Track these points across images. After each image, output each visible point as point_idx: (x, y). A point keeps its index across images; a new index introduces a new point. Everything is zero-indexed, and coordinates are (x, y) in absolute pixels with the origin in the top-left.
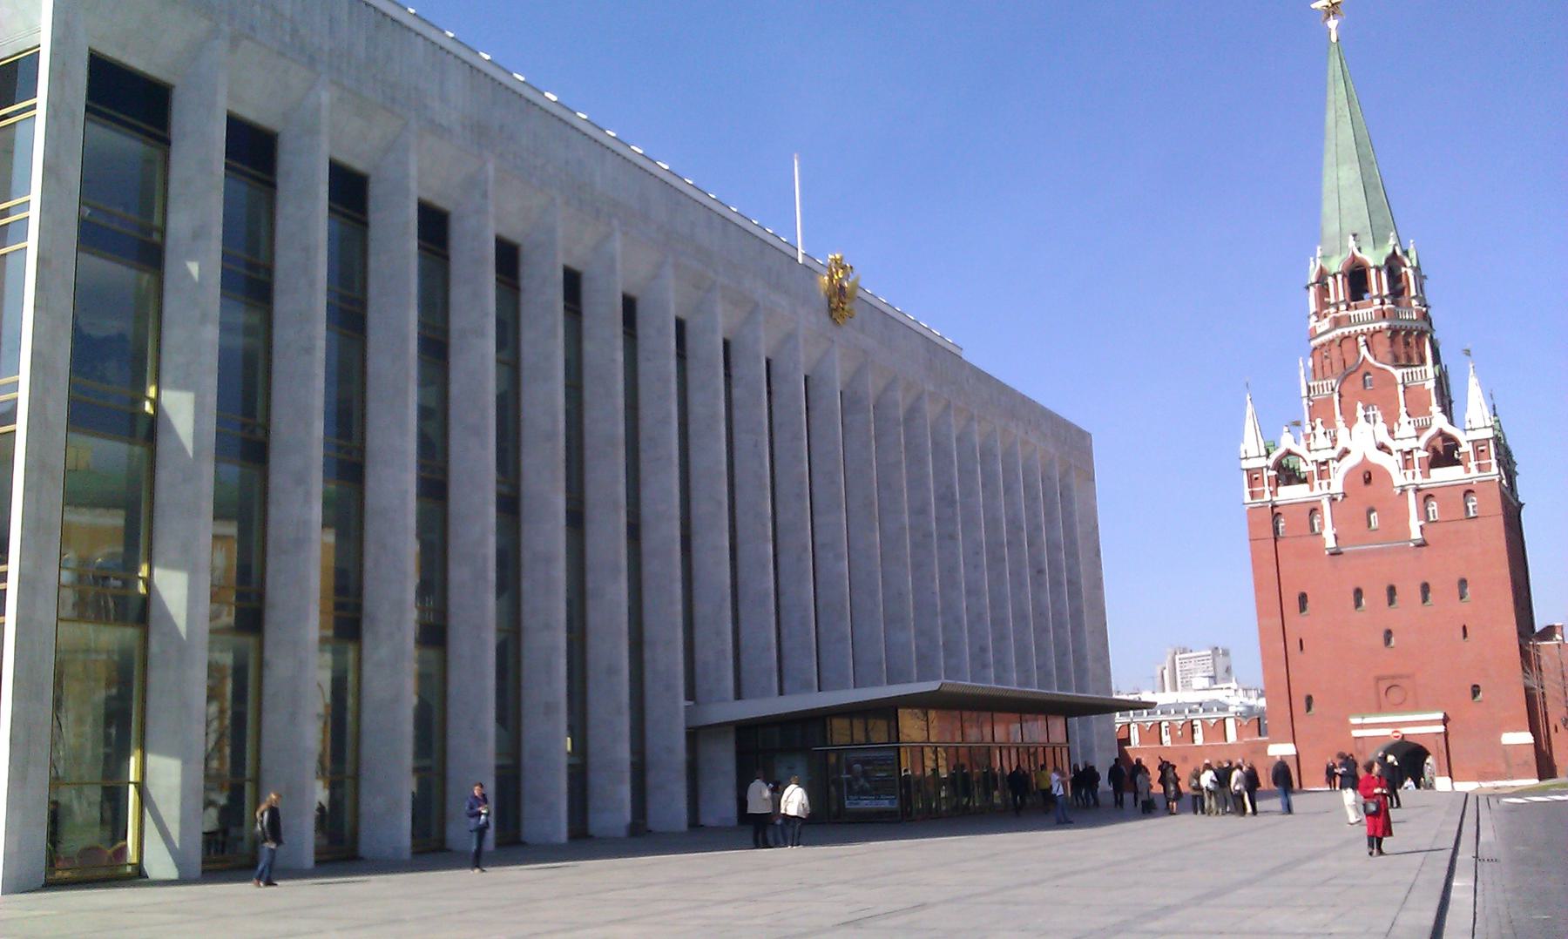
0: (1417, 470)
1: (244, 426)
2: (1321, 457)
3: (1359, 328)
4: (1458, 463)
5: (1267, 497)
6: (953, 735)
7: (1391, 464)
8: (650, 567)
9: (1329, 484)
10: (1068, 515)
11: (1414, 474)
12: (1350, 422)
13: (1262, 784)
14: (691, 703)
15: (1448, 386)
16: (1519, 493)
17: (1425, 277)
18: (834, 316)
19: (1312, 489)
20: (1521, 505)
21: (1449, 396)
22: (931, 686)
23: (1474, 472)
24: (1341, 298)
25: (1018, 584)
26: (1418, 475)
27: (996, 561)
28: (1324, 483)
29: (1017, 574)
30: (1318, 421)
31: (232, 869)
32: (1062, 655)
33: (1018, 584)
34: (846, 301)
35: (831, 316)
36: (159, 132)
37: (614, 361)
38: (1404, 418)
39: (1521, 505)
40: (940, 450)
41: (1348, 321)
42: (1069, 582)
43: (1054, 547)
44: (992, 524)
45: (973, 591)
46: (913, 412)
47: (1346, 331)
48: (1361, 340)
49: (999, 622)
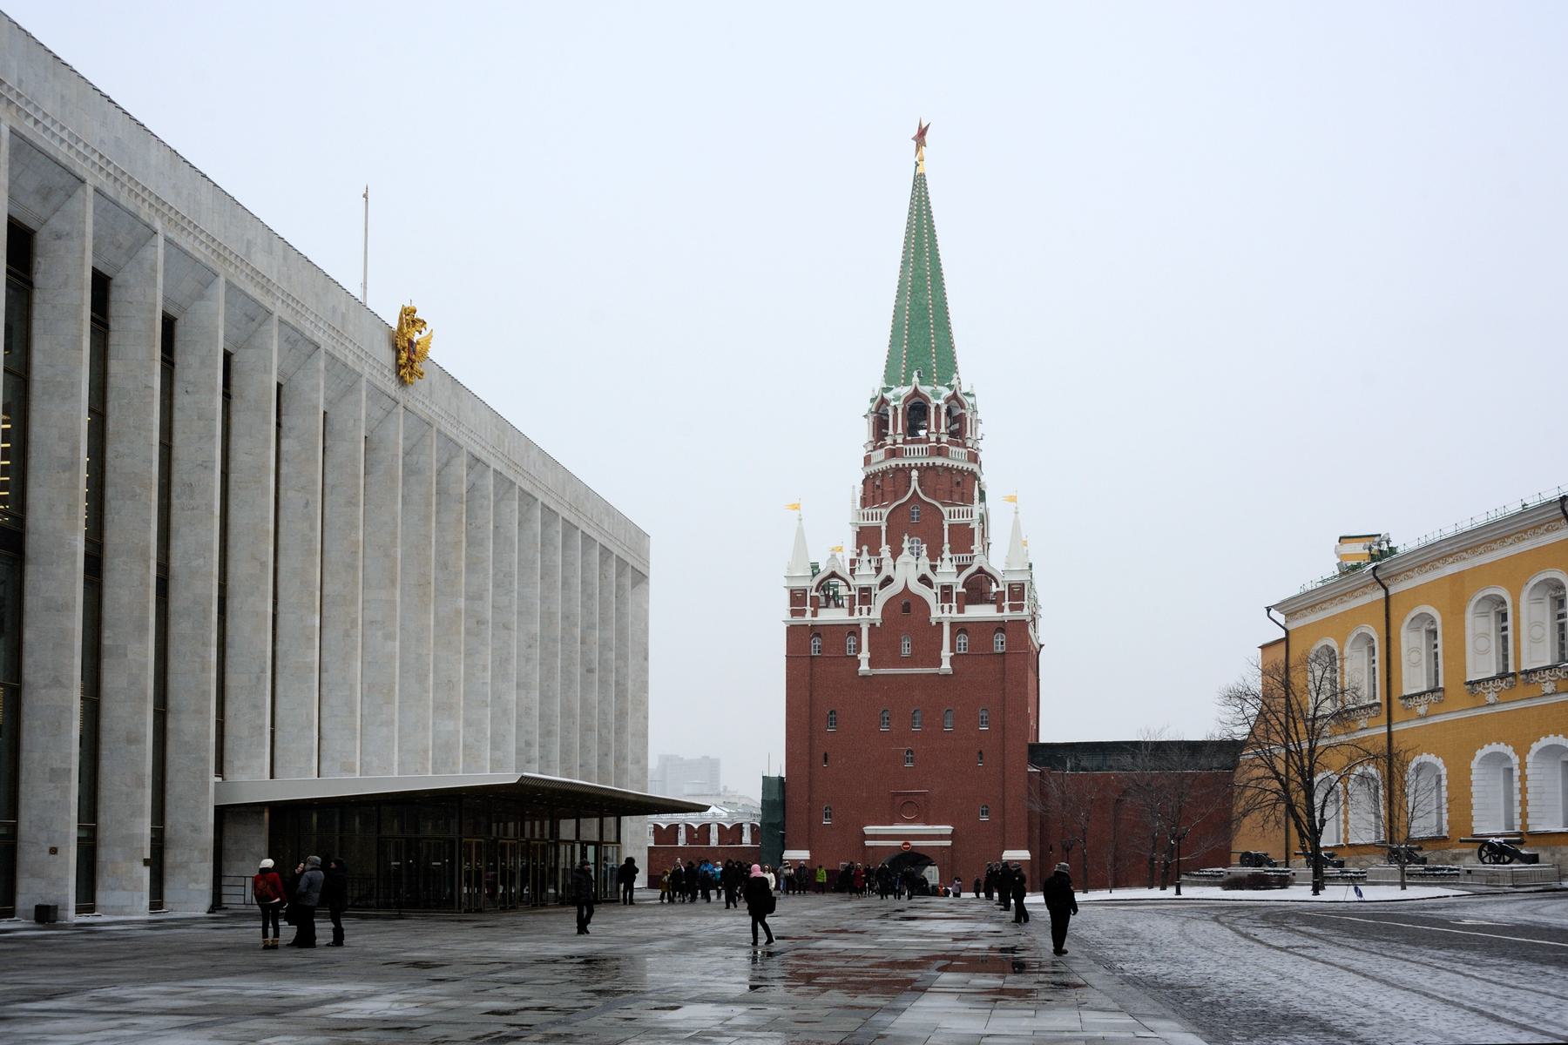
0: (954, 604)
2: (864, 583)
5: (808, 615)
7: (929, 595)
8: (179, 627)
9: (869, 610)
11: (951, 607)
12: (896, 553)
14: (220, 779)
18: (401, 373)
19: (851, 613)
26: (955, 610)
28: (865, 608)
29: (567, 672)
30: (865, 548)
35: (398, 373)
37: (149, 387)
42: (617, 683)
43: (604, 645)
47: (900, 462)
48: (915, 474)
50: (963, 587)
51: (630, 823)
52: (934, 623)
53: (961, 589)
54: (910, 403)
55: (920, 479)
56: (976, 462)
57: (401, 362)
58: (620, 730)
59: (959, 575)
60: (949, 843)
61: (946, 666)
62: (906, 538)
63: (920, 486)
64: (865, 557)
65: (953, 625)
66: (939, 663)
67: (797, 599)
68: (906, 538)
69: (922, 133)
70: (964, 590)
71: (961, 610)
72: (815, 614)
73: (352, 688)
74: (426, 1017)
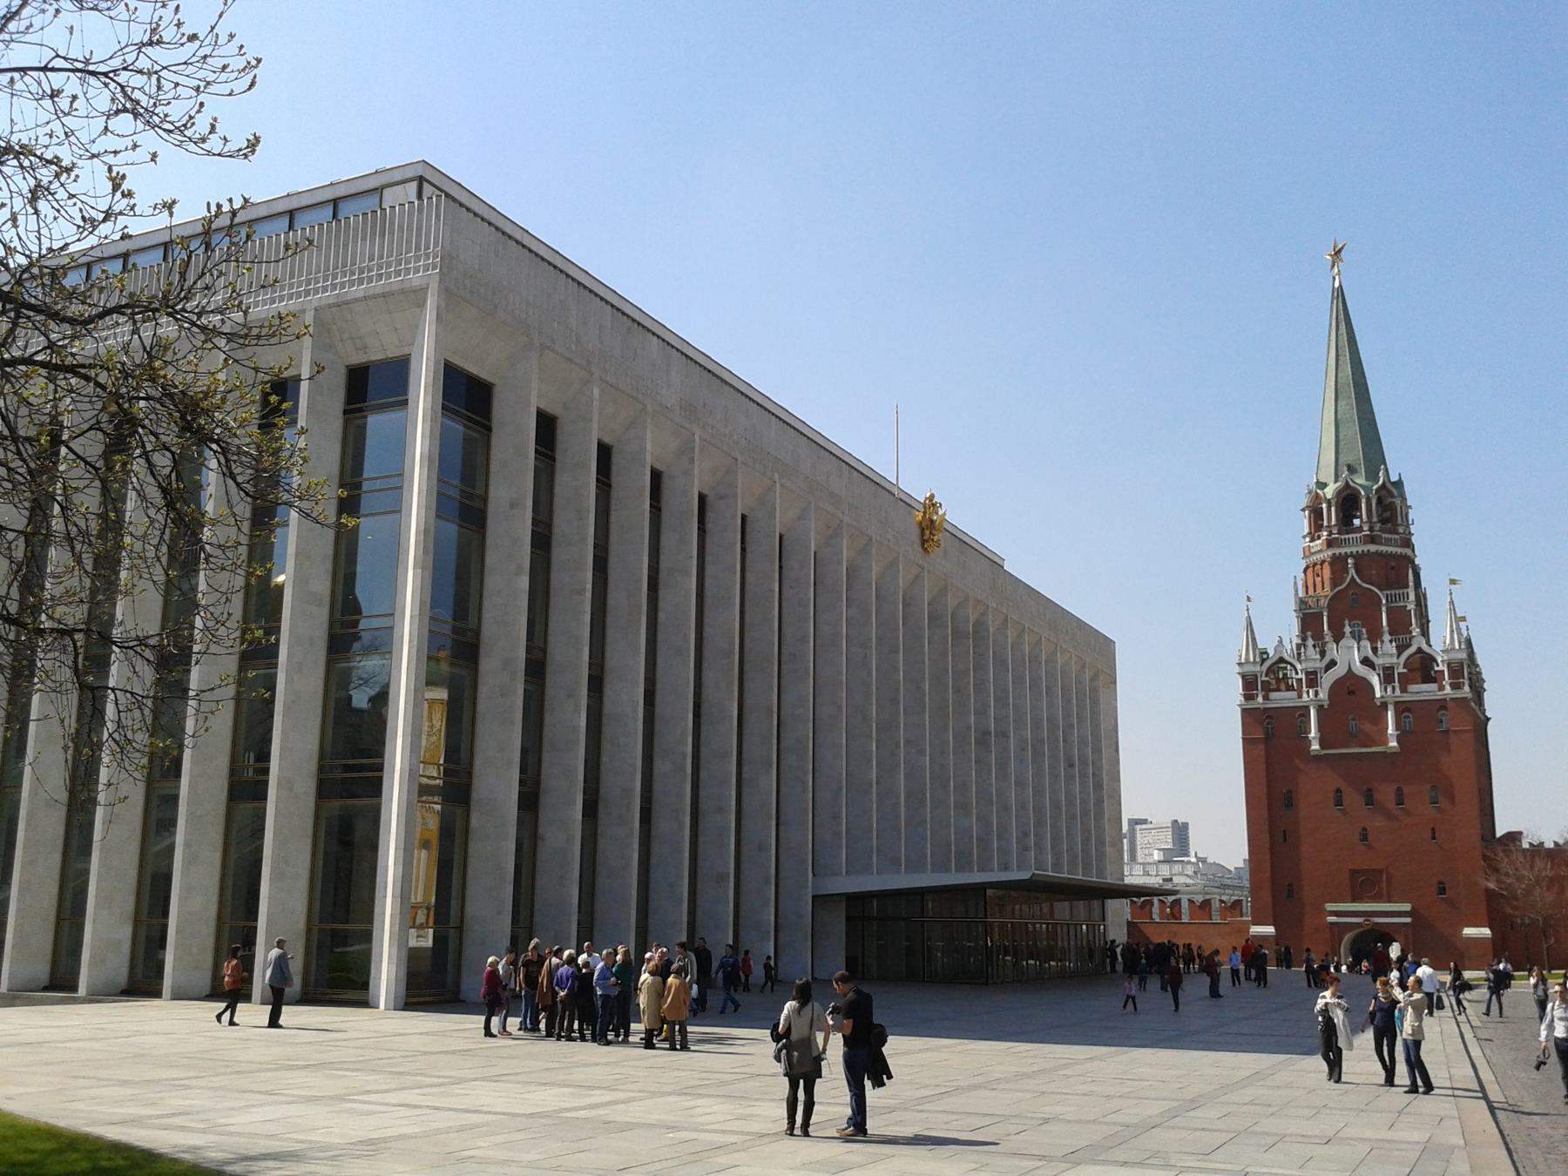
0: (1397, 684)
1: (455, 630)
2: (1311, 666)
3: (1348, 550)
4: (1433, 680)
5: (1260, 699)
6: (1021, 909)
10: (1095, 713)
11: (1394, 688)
12: (1338, 637)
13: (80, 990)
15: (1426, 606)
16: (1486, 707)
17: (1410, 507)
20: (1488, 719)
21: (1427, 616)
22: (1025, 875)
23: (1448, 689)
24: (1333, 523)
25: (1055, 777)
27: (1038, 755)
28: (1311, 692)
31: (441, 1002)
32: (1086, 840)
33: (1055, 777)
34: (935, 533)
35: (923, 545)
36: (549, 453)
38: (1387, 637)
39: (1488, 719)
40: (1000, 662)
41: (1346, 542)
43: (1083, 742)
44: (1037, 724)
45: (1020, 783)
46: (1051, 660)
49: (1039, 810)
50: (1404, 668)
51: (1113, 905)
52: (1378, 704)
53: (1402, 670)
54: (1343, 495)
55: (1356, 566)
56: (1408, 546)
57: (925, 538)
58: (1099, 815)
59: (1399, 656)
60: (1408, 920)
61: (1393, 744)
62: (1347, 622)
63: (1357, 572)
64: (1310, 642)
65: (1396, 704)
66: (1385, 742)
67: (1249, 683)
68: (1347, 622)
69: (1338, 252)
70: (1405, 670)
71: (1404, 690)
72: (1266, 698)
73: (898, 797)
74: (773, 1140)
